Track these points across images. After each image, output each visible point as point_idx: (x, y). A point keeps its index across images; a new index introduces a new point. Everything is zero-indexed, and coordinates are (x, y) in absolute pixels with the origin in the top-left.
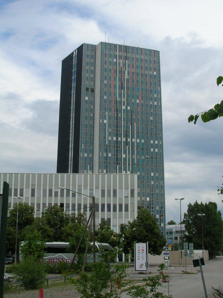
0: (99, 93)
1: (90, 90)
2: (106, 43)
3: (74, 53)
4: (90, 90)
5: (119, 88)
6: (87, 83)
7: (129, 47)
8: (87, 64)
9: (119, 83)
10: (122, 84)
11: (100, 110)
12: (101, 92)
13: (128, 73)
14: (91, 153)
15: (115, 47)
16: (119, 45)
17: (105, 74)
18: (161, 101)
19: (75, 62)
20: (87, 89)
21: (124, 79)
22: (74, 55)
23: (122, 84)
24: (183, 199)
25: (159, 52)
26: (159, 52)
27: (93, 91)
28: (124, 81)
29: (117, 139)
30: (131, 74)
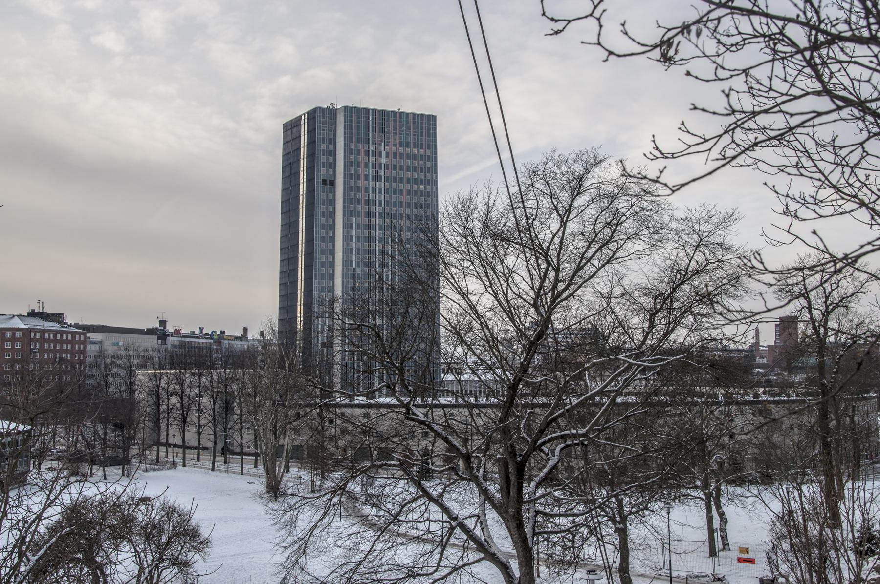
0: (342, 175)
1: (328, 182)
2: (352, 108)
3: (303, 118)
4: (328, 182)
5: (372, 180)
6: (323, 171)
7: (388, 112)
8: (323, 152)
9: (372, 172)
10: (377, 172)
11: (344, 215)
12: (344, 187)
13: (387, 154)
14: (331, 143)
15: (366, 114)
16: (373, 110)
17: (352, 183)
18: (437, 185)
19: (304, 129)
20: (324, 182)
21: (380, 164)
22: (302, 122)
23: (377, 172)
24: (604, 61)
25: (435, 117)
26: (435, 117)
27: (332, 183)
28: (380, 168)
29: (370, 233)
30: (391, 156)
